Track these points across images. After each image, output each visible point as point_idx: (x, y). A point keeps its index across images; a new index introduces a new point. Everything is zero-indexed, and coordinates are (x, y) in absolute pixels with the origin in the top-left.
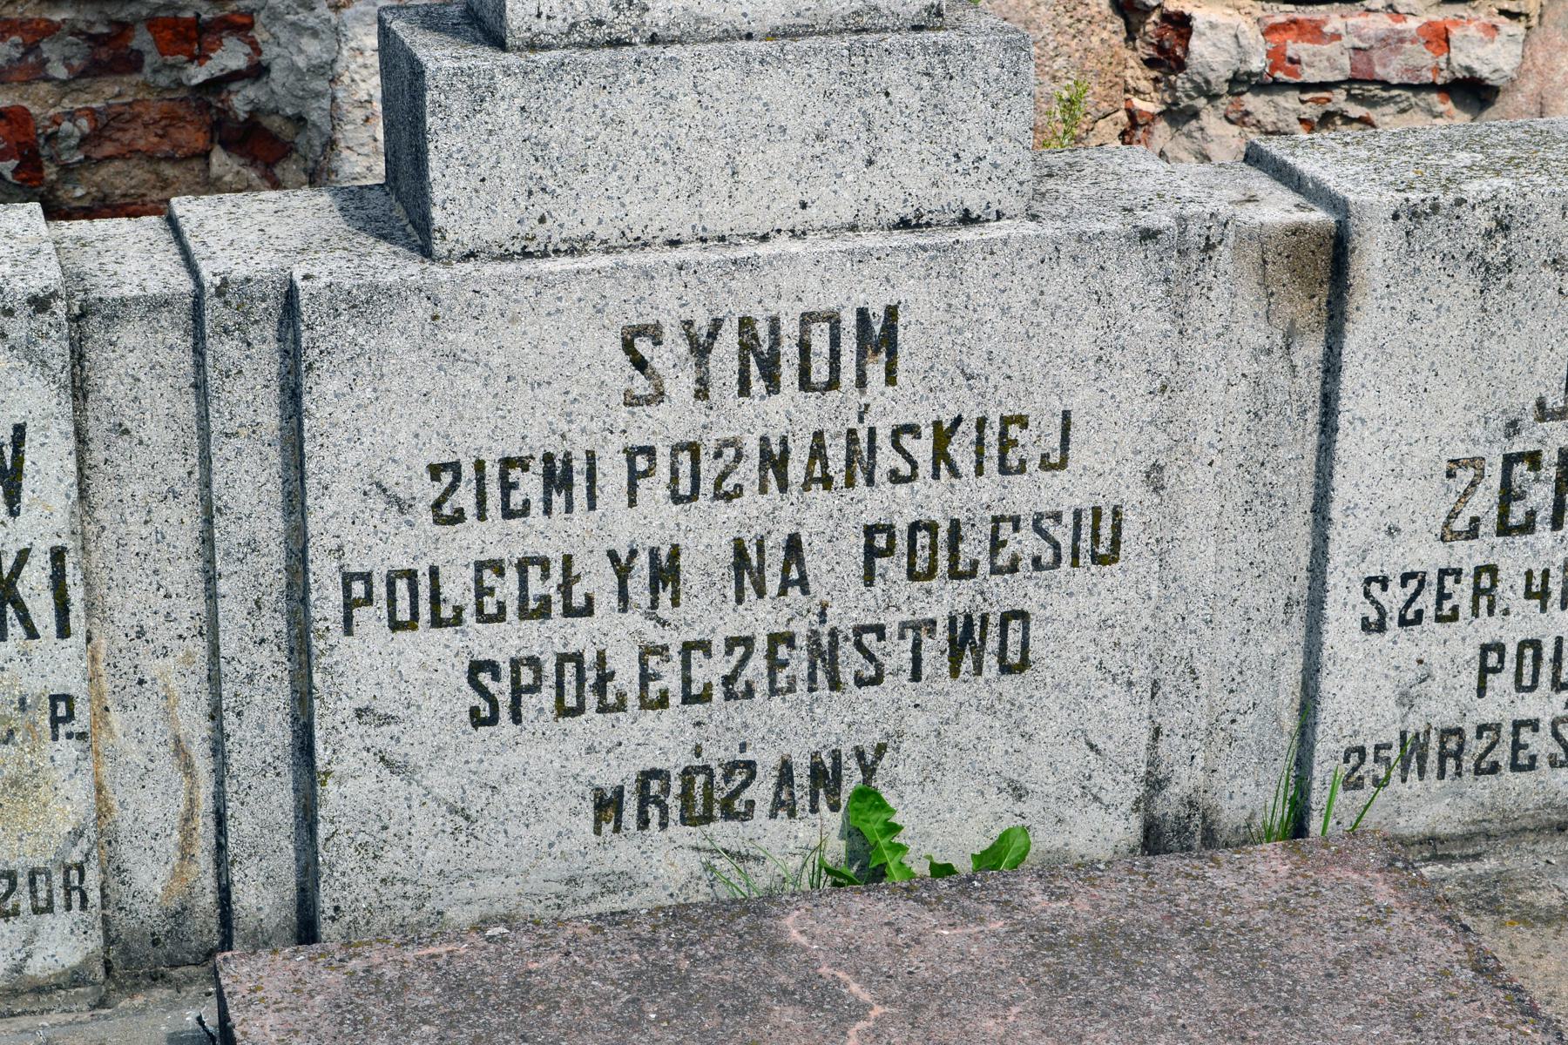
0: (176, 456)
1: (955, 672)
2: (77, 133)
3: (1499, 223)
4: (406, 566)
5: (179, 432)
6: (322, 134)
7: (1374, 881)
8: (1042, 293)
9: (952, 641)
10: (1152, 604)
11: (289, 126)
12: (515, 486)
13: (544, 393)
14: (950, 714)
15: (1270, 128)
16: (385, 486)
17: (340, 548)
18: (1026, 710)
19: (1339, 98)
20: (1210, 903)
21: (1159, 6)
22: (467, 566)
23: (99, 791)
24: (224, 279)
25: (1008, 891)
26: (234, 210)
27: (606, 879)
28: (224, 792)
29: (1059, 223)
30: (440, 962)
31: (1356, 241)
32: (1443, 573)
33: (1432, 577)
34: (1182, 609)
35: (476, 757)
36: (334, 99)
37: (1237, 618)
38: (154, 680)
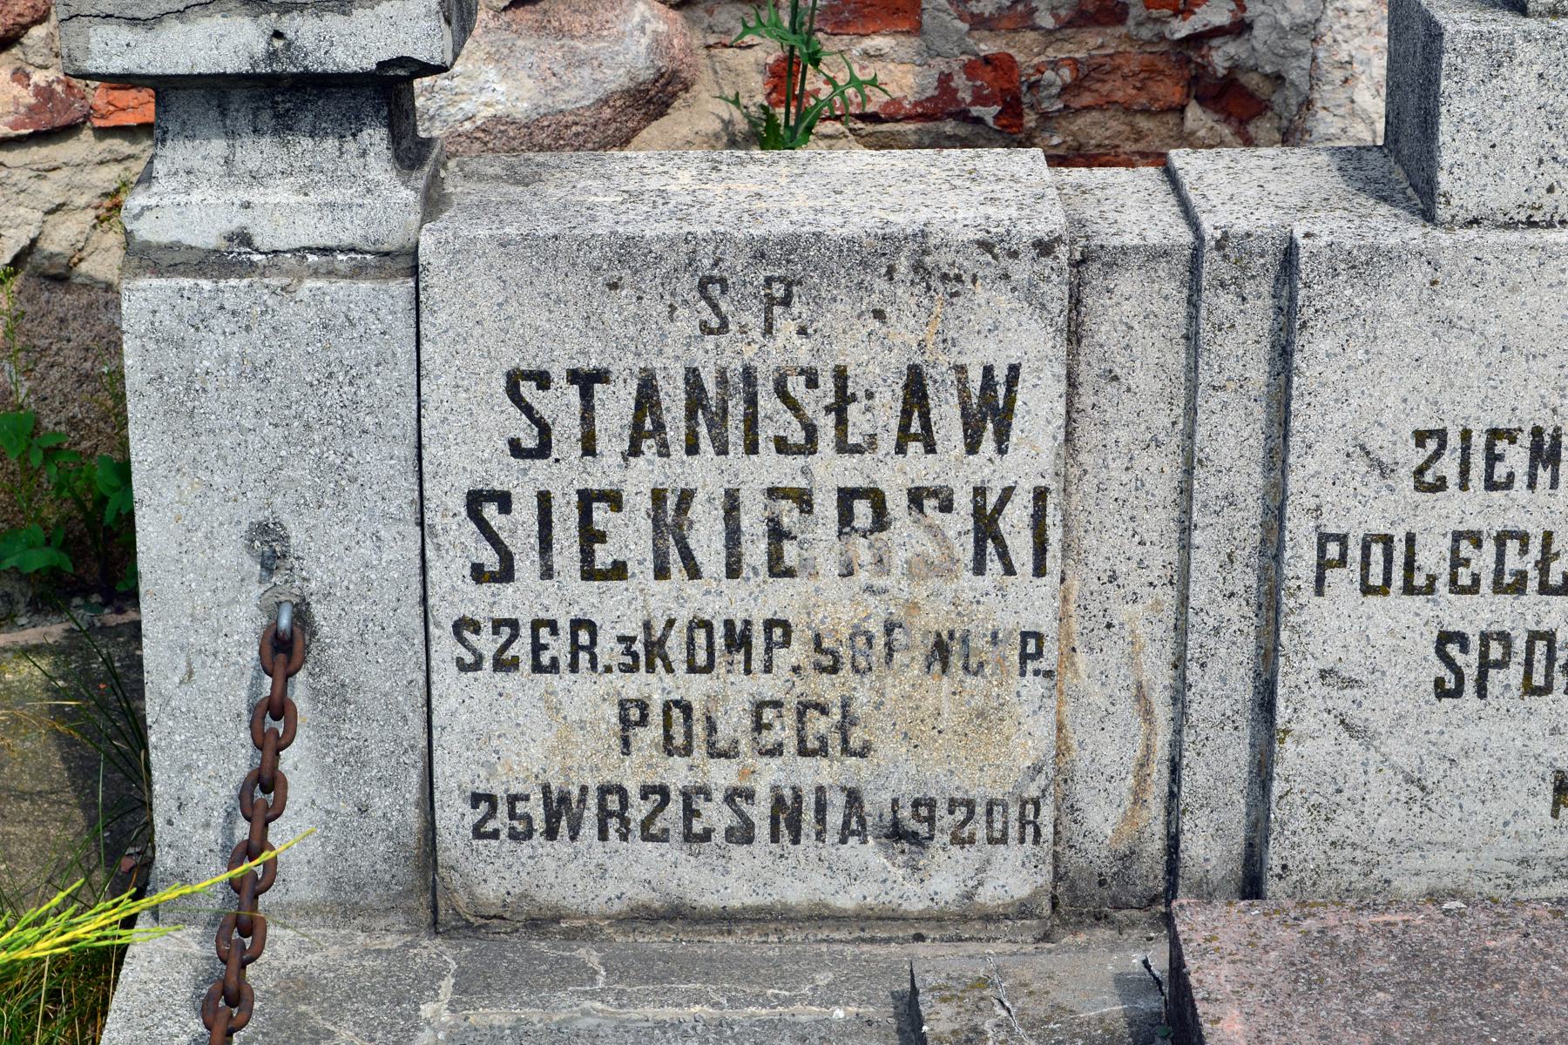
0: (1162, 405)
2: (1059, 82)
4: (1383, 531)
5: (1167, 382)
6: (1299, 93)
11: (1267, 83)
12: (1500, 458)
13: (1538, 365)
16: (1369, 449)
17: (1318, 508)
22: (1445, 535)
23: (1060, 729)
24: (1225, 233)
26: (1232, 164)
27: (1559, 863)
28: (1181, 742)
30: (1396, 930)
35: (1437, 728)
36: (1314, 59)
38: (1122, 624)
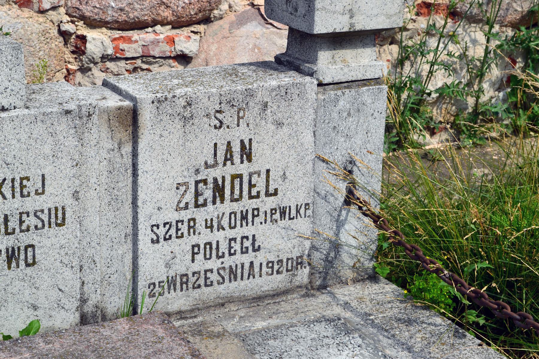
1: (9, 268)
3: (188, 103)
7: (158, 328)
8: (32, 134)
9: (8, 257)
10: (78, 239)
14: (8, 282)
15: (116, 73)
18: (36, 279)
19: (139, 62)
20: (102, 341)
21: (75, 33)
25: (31, 343)
29: (36, 109)
31: (140, 111)
32: (177, 222)
33: (174, 223)
34: (89, 240)
37: (108, 242)
